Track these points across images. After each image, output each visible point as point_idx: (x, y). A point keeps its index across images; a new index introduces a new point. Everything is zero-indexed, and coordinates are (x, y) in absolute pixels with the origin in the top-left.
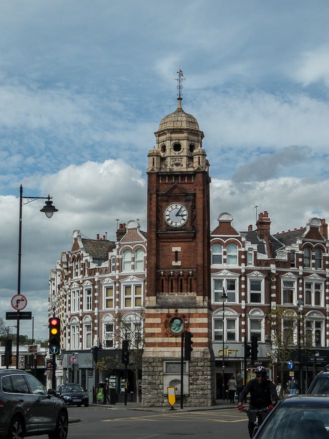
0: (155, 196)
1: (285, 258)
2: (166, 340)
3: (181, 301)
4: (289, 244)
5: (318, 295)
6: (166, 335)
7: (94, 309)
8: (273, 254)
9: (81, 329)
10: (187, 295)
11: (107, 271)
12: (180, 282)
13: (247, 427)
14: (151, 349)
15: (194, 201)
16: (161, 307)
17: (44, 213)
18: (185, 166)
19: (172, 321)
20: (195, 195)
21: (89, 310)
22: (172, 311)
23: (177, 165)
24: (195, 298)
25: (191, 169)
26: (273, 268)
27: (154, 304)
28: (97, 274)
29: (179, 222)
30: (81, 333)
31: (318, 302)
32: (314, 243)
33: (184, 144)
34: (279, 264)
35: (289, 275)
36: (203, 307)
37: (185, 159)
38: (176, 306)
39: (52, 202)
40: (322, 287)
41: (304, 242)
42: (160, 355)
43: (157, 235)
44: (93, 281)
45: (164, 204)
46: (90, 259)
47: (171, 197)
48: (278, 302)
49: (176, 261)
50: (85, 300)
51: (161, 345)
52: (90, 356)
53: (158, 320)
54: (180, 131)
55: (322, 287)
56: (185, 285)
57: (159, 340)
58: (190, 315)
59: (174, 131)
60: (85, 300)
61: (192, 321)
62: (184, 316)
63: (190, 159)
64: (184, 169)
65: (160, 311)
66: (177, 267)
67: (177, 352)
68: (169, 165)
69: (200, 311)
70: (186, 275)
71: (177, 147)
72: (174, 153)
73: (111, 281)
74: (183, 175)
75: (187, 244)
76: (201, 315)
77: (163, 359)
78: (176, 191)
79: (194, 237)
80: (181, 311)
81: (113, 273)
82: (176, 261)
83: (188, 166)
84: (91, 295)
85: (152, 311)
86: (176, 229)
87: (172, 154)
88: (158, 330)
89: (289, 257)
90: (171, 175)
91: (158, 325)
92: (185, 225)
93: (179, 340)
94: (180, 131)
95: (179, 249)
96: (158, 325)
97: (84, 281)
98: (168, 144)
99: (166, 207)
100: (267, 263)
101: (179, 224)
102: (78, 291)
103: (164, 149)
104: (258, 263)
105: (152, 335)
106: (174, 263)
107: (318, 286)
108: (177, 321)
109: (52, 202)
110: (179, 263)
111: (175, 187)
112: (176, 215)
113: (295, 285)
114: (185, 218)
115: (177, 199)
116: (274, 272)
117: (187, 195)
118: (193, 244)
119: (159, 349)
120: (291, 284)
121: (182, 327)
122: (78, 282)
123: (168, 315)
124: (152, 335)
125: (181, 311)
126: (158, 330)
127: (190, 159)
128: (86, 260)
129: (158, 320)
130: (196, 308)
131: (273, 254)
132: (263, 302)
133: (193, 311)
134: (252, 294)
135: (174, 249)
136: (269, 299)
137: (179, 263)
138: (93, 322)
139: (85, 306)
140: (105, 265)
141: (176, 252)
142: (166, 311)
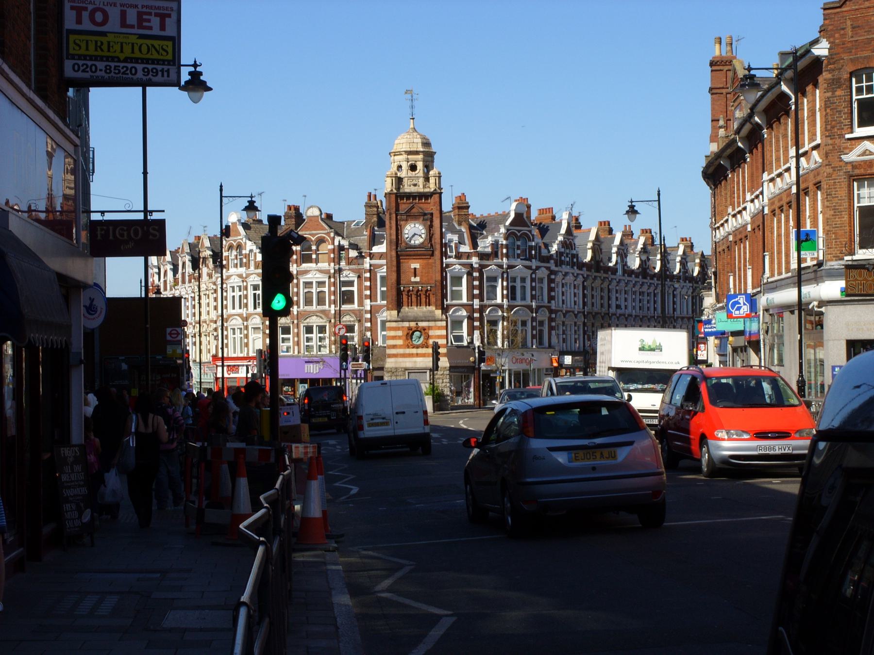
0: (394, 215)
1: (489, 250)
2: (408, 351)
3: (421, 314)
4: (492, 232)
5: (523, 288)
7: (330, 306)
8: (475, 245)
9: (246, 332)
10: (425, 309)
12: (421, 297)
13: (110, 19)
15: (432, 221)
16: (403, 321)
17: (186, 93)
18: (421, 186)
19: (413, 334)
20: (432, 214)
22: (413, 324)
23: (415, 185)
24: (433, 312)
25: (427, 190)
26: (475, 260)
29: (418, 241)
30: (247, 336)
31: (523, 298)
32: (519, 231)
33: (420, 165)
34: (483, 256)
36: (441, 320)
38: (416, 320)
39: (201, 73)
41: (508, 230)
45: (402, 223)
47: (410, 216)
51: (404, 356)
53: (400, 333)
54: (417, 153)
55: (528, 281)
56: (423, 300)
57: (401, 351)
58: (430, 328)
59: (410, 153)
63: (427, 179)
64: (420, 189)
65: (401, 324)
66: (416, 283)
67: (428, 362)
68: (407, 188)
69: (439, 324)
70: (415, 290)
71: (413, 168)
72: (411, 174)
75: (425, 261)
76: (440, 328)
77: (406, 369)
78: (414, 210)
79: (432, 255)
80: (421, 324)
83: (424, 187)
85: (394, 324)
86: (415, 247)
87: (409, 175)
88: (400, 342)
89: (492, 248)
92: (423, 243)
93: (143, 296)
94: (417, 153)
95: (417, 266)
97: (248, 275)
98: (405, 166)
99: (405, 225)
100: (469, 256)
101: (417, 242)
102: (240, 287)
105: (394, 347)
106: (413, 279)
107: (523, 280)
108: (417, 334)
109: (201, 73)
110: (418, 279)
111: (412, 208)
114: (423, 236)
117: (425, 214)
118: (430, 261)
119: (400, 359)
121: (422, 339)
122: (240, 276)
123: (410, 328)
124: (394, 347)
125: (421, 324)
126: (400, 342)
127: (427, 179)
129: (400, 333)
131: (475, 245)
132: (464, 300)
133: (431, 324)
135: (413, 266)
136: (471, 297)
137: (418, 279)
141: (415, 269)
142: (406, 324)
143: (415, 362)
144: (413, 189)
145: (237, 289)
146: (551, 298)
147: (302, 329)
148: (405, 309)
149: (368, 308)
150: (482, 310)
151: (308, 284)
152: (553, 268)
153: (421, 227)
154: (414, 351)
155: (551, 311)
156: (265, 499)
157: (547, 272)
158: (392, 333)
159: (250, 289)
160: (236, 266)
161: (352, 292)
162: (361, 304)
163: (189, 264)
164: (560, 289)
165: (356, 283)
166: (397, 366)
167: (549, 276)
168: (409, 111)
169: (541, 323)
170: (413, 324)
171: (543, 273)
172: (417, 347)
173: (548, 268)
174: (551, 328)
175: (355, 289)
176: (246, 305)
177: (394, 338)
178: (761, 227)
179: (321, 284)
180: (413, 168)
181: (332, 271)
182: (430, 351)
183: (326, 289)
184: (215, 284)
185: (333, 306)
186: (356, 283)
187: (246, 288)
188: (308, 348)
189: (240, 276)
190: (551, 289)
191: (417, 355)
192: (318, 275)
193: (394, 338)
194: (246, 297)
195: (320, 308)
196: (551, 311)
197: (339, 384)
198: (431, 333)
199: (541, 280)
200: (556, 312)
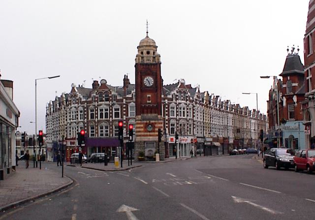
0: (139, 73)
2: (146, 134)
5: (184, 112)
6: (146, 132)
10: (154, 115)
11: (91, 102)
14: (139, 137)
16: (143, 120)
21: (82, 120)
22: (148, 122)
23: (149, 60)
24: (157, 116)
27: (140, 119)
28: (86, 104)
34: (169, 99)
35: (173, 105)
36: (161, 120)
37: (152, 58)
38: (149, 119)
40: (186, 109)
42: (144, 140)
43: (141, 90)
44: (83, 107)
46: (82, 97)
48: (169, 116)
49: (149, 100)
50: (79, 115)
51: (144, 136)
52: (250, 138)
53: (142, 126)
55: (186, 109)
57: (143, 134)
58: (155, 123)
60: (79, 115)
61: (156, 125)
62: (153, 123)
64: (151, 62)
65: (143, 122)
67: (156, 138)
69: (160, 121)
71: (148, 53)
73: (93, 107)
74: (151, 64)
77: (145, 142)
81: (94, 104)
82: (149, 100)
83: (153, 61)
84: (83, 113)
86: (147, 87)
88: (142, 130)
90: (147, 64)
91: (142, 127)
95: (150, 96)
96: (142, 127)
97: (78, 107)
98: (145, 52)
103: (142, 53)
104: (118, 101)
106: (148, 102)
110: (150, 102)
112: (149, 81)
113: (175, 108)
115: (149, 75)
116: (167, 103)
119: (142, 137)
120: (173, 108)
122: (75, 107)
123: (146, 123)
124: (139, 132)
125: (151, 122)
126: (142, 130)
128: (79, 97)
129: (142, 126)
130: (158, 120)
133: (156, 121)
134: (115, 113)
135: (148, 96)
138: (84, 125)
139: (79, 118)
140: (90, 99)
141: (149, 97)
142: (145, 122)
143: (149, 139)
144: (148, 62)
145: (74, 112)
146: (194, 116)
147: (99, 128)
148: (83, 165)
149: (125, 119)
150: (169, 120)
151: (101, 110)
152: (194, 105)
153: (152, 79)
154: (149, 134)
155: (194, 121)
156: (119, 117)
157: (192, 106)
158: (139, 126)
159: (79, 112)
160: (74, 104)
161: (119, 113)
162: (122, 117)
163: (58, 105)
164: (196, 113)
165: (120, 109)
166: (141, 140)
167: (193, 108)
168: (146, 29)
169: (190, 125)
170: (148, 122)
171: (191, 106)
172: (150, 132)
173: (192, 105)
174: (194, 128)
175: (120, 111)
176: (77, 118)
177: (139, 128)
178: (72, 141)
179: (106, 110)
180: (148, 53)
181: (111, 105)
182: (157, 133)
183: (108, 112)
184: (66, 111)
185: (111, 118)
186: (120, 109)
187: (77, 112)
188: (102, 135)
189: (75, 107)
190: (193, 113)
191: (150, 135)
192: (105, 106)
193: (139, 128)
194: (77, 115)
195: (106, 119)
196: (194, 121)
197: (83, 132)
198: (156, 125)
199: (190, 109)
200: (195, 121)
